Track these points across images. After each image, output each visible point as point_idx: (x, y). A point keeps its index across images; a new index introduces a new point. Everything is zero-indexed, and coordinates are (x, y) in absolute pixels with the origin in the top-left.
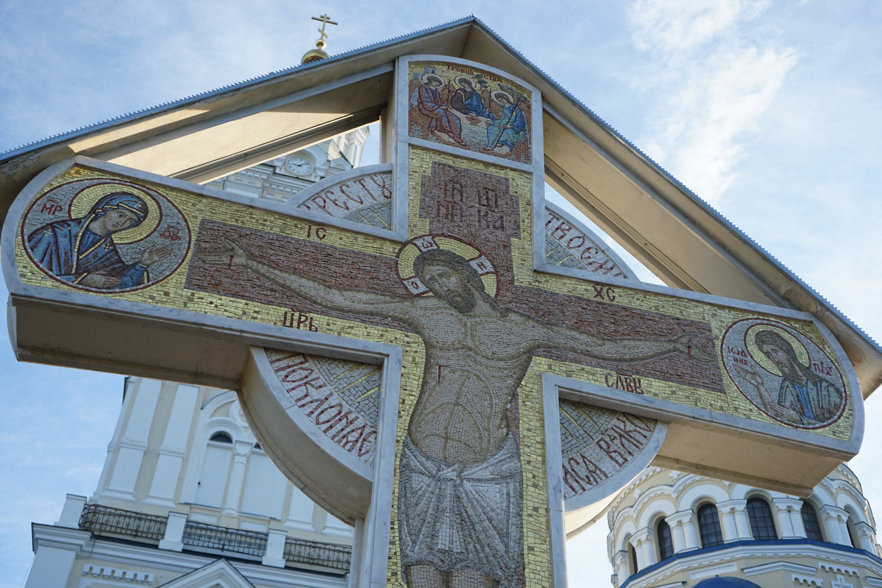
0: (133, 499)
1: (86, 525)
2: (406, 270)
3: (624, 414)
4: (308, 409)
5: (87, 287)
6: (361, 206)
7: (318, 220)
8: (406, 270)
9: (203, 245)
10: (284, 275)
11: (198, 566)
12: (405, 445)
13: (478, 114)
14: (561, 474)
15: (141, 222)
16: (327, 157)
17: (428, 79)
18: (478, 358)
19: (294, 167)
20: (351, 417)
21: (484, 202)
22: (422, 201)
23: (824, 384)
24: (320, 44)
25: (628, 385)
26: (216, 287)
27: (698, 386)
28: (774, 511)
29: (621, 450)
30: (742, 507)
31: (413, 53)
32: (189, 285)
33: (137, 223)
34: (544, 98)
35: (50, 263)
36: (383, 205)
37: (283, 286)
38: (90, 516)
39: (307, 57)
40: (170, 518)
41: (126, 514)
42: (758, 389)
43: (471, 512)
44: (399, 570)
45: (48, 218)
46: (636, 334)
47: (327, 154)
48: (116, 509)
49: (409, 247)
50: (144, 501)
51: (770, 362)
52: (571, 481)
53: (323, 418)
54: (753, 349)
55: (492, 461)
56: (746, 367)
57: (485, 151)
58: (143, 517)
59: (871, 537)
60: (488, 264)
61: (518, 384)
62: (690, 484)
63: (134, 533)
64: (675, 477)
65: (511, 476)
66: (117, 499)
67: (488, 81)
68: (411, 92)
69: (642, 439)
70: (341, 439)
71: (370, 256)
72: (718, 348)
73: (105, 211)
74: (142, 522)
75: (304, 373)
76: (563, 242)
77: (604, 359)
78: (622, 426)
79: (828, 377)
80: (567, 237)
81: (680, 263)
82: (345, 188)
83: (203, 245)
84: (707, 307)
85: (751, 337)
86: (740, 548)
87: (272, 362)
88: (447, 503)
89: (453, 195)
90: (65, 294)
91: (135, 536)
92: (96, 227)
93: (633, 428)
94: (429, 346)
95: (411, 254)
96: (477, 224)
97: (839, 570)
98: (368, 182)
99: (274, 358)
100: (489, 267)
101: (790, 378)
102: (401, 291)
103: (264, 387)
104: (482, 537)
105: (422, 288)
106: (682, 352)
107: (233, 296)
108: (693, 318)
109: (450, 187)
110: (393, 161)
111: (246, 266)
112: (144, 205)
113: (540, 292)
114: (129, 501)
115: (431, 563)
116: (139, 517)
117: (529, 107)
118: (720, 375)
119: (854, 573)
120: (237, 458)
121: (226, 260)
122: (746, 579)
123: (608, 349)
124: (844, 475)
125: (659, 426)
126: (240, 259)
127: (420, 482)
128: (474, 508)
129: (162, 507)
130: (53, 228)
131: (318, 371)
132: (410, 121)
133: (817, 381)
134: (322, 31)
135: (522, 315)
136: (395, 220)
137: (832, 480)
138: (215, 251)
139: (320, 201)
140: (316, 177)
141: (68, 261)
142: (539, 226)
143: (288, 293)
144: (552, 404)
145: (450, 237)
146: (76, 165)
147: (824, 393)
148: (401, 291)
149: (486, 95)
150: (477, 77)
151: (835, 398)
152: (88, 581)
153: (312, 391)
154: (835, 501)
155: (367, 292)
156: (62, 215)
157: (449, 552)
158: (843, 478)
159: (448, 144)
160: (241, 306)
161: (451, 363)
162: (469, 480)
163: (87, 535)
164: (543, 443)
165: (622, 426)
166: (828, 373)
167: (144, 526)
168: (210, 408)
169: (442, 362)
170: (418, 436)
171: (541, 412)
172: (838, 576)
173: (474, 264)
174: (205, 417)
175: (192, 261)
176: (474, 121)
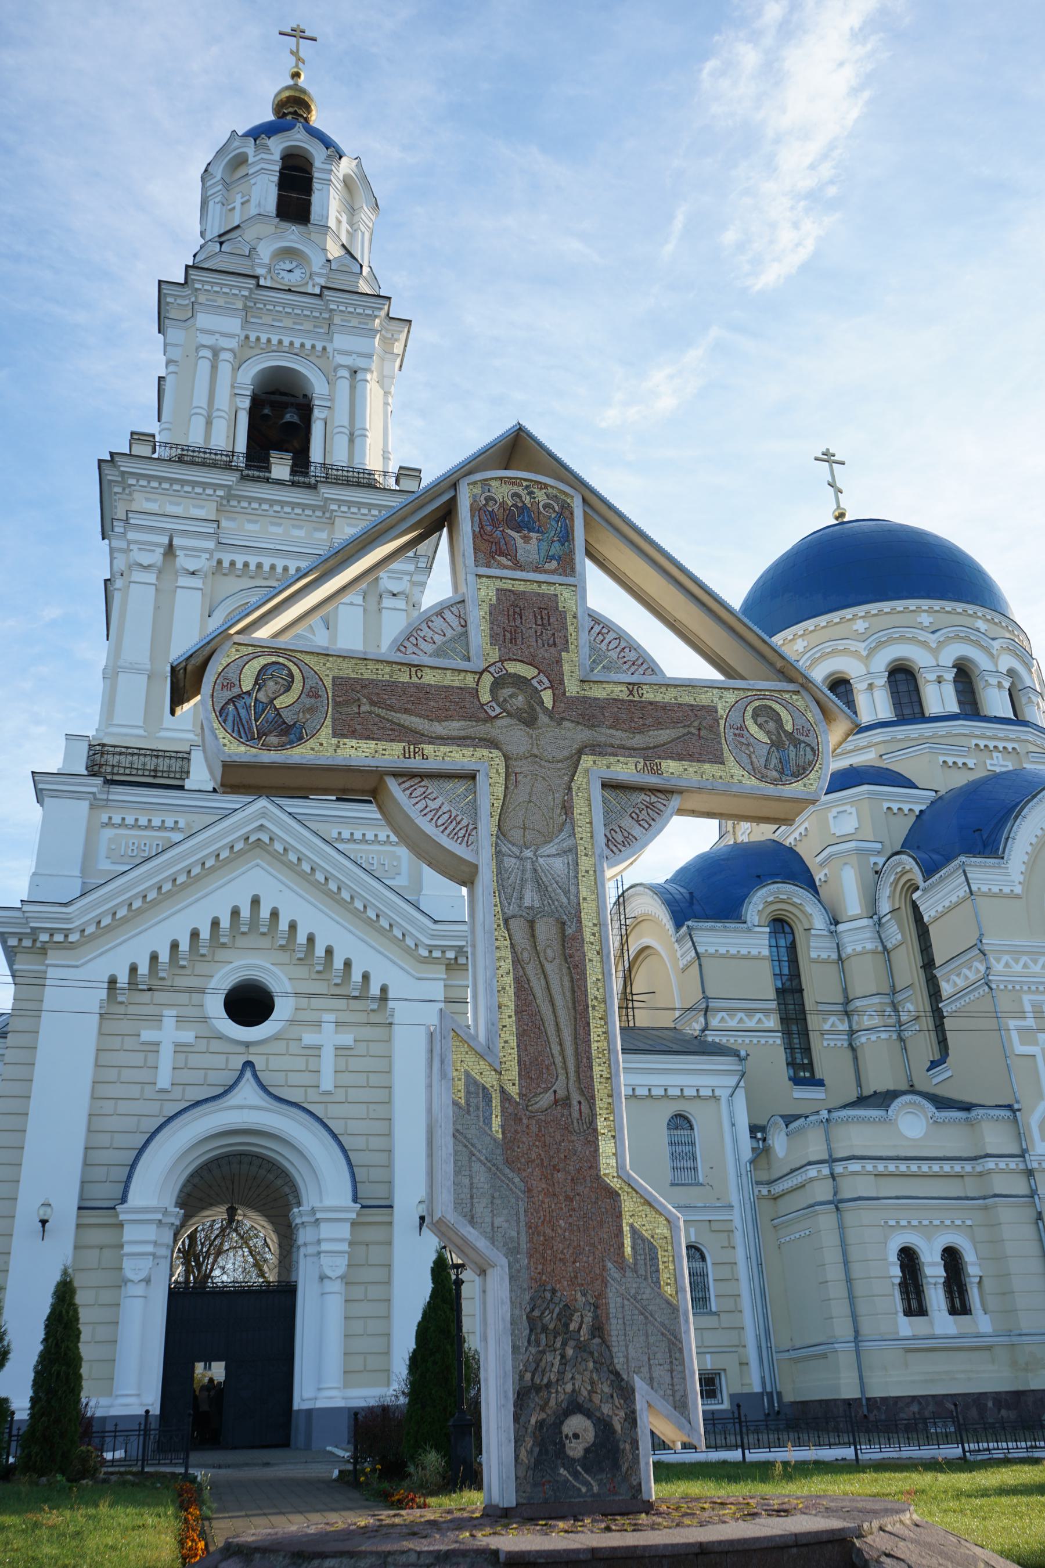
0: (145, 734)
1: (94, 769)
2: (485, 697)
3: (650, 790)
4: (429, 816)
5: (267, 747)
6: (445, 639)
7: (416, 663)
8: (485, 697)
9: (338, 699)
10: (398, 715)
11: (237, 806)
12: (497, 837)
13: (530, 531)
14: (604, 840)
15: (291, 687)
16: (326, 255)
17: (486, 499)
18: (543, 763)
19: (283, 274)
20: (459, 819)
21: (539, 622)
22: (491, 629)
23: (803, 745)
24: (296, 75)
25: (652, 768)
26: (353, 734)
27: (704, 762)
28: (921, 682)
29: (648, 818)
30: (882, 681)
31: (470, 473)
32: (335, 735)
33: (288, 689)
34: (584, 500)
35: (239, 731)
36: (462, 634)
37: (399, 725)
38: (97, 756)
39: (279, 98)
40: (193, 752)
41: (139, 752)
42: (750, 757)
43: (544, 879)
44: (501, 922)
45: (229, 694)
46: (658, 724)
47: (325, 250)
48: (127, 748)
49: (486, 675)
50: (158, 735)
51: (762, 732)
52: (611, 846)
53: (440, 822)
54: (750, 723)
55: (557, 841)
56: (742, 740)
57: (537, 569)
58: (161, 754)
59: (1038, 704)
60: (545, 680)
61: (572, 780)
62: (819, 658)
63: (152, 774)
64: (801, 650)
65: (570, 850)
66: (126, 735)
67: (536, 490)
68: (472, 516)
69: (662, 808)
70: (454, 836)
71: (457, 688)
72: (722, 727)
73: (264, 681)
74: (161, 760)
75: (423, 790)
76: (603, 646)
77: (634, 749)
78: (648, 799)
79: (806, 739)
80: (606, 641)
81: (702, 637)
82: (430, 624)
83: (338, 699)
84: (715, 691)
85: (750, 709)
86: (879, 730)
87: (400, 784)
88: (528, 875)
89: (515, 619)
90: (256, 756)
91: (155, 777)
92: (262, 696)
93: (656, 799)
94: (507, 758)
95: (487, 680)
96: (534, 644)
97: (995, 747)
98: (447, 614)
99: (400, 781)
100: (547, 684)
101: (776, 744)
102: (483, 715)
103: (398, 804)
104: (553, 895)
105: (498, 710)
106: (693, 734)
107: (366, 739)
108: (704, 703)
109: (511, 612)
110: (465, 590)
111: (370, 713)
112: (290, 670)
113: (586, 698)
115: (521, 916)
116: (156, 754)
117: (572, 514)
118: (722, 749)
119: (1014, 749)
121: (356, 710)
122: (885, 766)
123: (638, 741)
124: (1009, 631)
125: (675, 796)
126: (365, 708)
127: (510, 862)
128: (546, 875)
129: (181, 740)
130: (234, 702)
131: (431, 787)
132: (475, 549)
133: (796, 743)
134: (295, 53)
135: (572, 721)
136: (472, 653)
137: (993, 639)
138: (347, 703)
139: (412, 639)
140: (314, 286)
141: (251, 728)
142: (584, 638)
143: (404, 730)
144: (597, 792)
145: (515, 660)
146: (235, 643)
147: (802, 753)
148: (483, 715)
149: (535, 508)
150: (527, 487)
151: (809, 756)
152: (109, 833)
153: (430, 802)
154: (996, 665)
155: (459, 720)
156: (236, 691)
157: (531, 908)
158: (1008, 635)
159: (506, 567)
160: (373, 746)
161: (523, 769)
162: (542, 857)
163: (99, 781)
164: (591, 823)
165: (648, 799)
166: (807, 736)
167: (163, 764)
169: (517, 770)
170: (505, 829)
171: (589, 800)
172: (995, 754)
173: (534, 682)
175: (333, 715)
176: (526, 539)
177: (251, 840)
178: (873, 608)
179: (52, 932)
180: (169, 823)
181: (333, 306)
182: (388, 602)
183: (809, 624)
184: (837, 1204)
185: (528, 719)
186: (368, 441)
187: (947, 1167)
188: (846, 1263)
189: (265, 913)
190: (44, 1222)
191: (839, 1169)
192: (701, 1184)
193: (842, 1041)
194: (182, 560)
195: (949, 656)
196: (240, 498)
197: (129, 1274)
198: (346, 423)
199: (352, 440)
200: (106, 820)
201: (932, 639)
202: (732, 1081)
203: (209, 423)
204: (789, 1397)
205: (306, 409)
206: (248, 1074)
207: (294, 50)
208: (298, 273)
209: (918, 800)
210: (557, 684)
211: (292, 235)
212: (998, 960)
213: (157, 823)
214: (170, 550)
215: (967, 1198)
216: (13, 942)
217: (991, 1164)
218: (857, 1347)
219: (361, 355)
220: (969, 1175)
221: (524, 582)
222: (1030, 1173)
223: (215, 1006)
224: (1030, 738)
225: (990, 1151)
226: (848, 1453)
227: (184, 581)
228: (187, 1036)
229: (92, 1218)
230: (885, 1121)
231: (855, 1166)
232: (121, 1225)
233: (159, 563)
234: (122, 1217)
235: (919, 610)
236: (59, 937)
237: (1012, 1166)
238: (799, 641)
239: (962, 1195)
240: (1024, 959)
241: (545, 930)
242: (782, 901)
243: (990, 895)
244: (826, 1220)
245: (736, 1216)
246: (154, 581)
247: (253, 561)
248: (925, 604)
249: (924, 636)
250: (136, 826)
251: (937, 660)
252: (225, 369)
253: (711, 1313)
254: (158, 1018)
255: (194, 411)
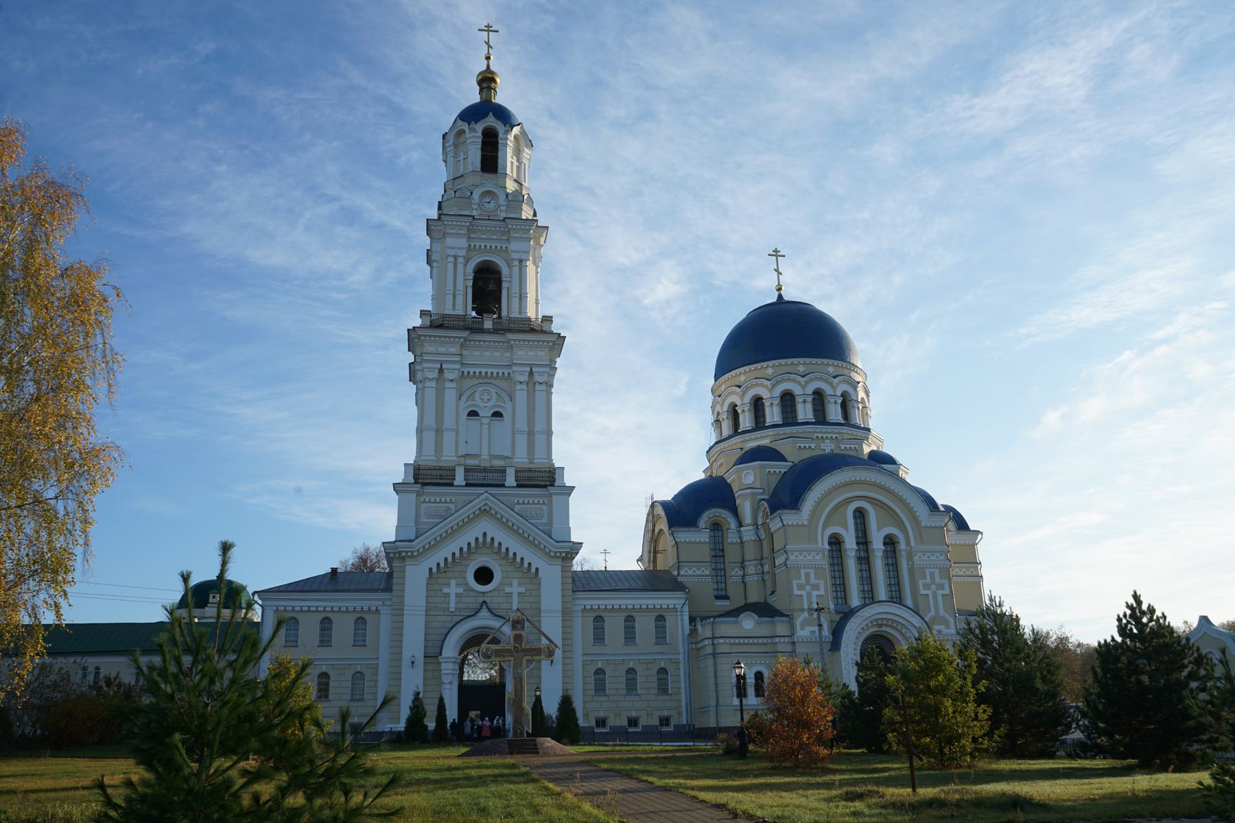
30: (777, 401)
41: (434, 469)
66: (428, 460)
91: (441, 479)
114: (433, 460)
116: (440, 469)
120: (483, 426)
152: (424, 506)
154: (835, 392)
167: (444, 473)
168: (464, 397)
174: (462, 404)
177: (482, 509)
178: (776, 362)
179: (407, 552)
180: (448, 500)
181: (510, 227)
182: (538, 387)
183: (747, 368)
184: (714, 655)
185: (517, 652)
186: (528, 299)
187: (760, 641)
188: (716, 677)
189: (489, 540)
190: (413, 663)
191: (716, 641)
192: (667, 644)
193: (740, 580)
194: (448, 375)
195: (810, 389)
196: (470, 341)
197: (444, 681)
198: (518, 291)
199: (520, 299)
200: (423, 500)
201: (802, 380)
202: (683, 601)
203: (454, 296)
204: (697, 726)
205: (499, 282)
206: (484, 606)
207: (490, 49)
208: (492, 202)
209: (784, 467)
210: (521, 647)
211: (489, 182)
212: (792, 554)
213: (443, 500)
214: (441, 370)
215: (767, 653)
216: (391, 555)
217: (777, 640)
218: (717, 709)
219: (523, 252)
220: (769, 643)
221: (518, 632)
222: (794, 643)
223: (470, 578)
224: (845, 431)
225: (778, 634)
226: (660, 744)
227: (448, 385)
228: (460, 590)
229: (429, 660)
230: (736, 623)
231: (722, 641)
232: (440, 663)
233: (437, 377)
234: (440, 660)
235: (799, 363)
236: (409, 554)
237: (786, 640)
238: (742, 376)
239: (765, 651)
240: (805, 553)
241: (518, 680)
242: (717, 516)
243: (792, 526)
244: (710, 661)
245: (681, 657)
246: (435, 386)
247: (477, 371)
248: (802, 360)
249: (799, 378)
250: (435, 502)
251: (804, 391)
252: (460, 267)
253: (669, 695)
254: (448, 585)
255: (447, 292)
